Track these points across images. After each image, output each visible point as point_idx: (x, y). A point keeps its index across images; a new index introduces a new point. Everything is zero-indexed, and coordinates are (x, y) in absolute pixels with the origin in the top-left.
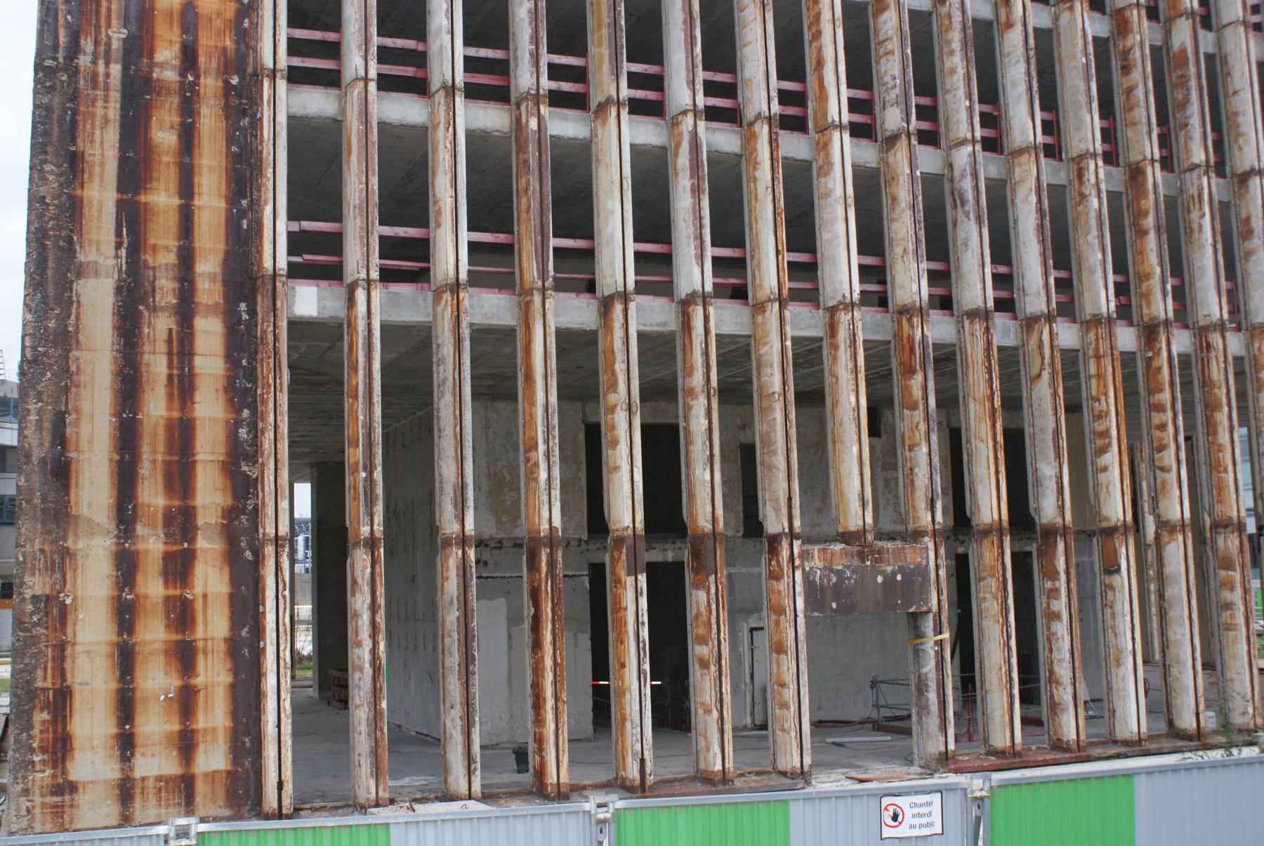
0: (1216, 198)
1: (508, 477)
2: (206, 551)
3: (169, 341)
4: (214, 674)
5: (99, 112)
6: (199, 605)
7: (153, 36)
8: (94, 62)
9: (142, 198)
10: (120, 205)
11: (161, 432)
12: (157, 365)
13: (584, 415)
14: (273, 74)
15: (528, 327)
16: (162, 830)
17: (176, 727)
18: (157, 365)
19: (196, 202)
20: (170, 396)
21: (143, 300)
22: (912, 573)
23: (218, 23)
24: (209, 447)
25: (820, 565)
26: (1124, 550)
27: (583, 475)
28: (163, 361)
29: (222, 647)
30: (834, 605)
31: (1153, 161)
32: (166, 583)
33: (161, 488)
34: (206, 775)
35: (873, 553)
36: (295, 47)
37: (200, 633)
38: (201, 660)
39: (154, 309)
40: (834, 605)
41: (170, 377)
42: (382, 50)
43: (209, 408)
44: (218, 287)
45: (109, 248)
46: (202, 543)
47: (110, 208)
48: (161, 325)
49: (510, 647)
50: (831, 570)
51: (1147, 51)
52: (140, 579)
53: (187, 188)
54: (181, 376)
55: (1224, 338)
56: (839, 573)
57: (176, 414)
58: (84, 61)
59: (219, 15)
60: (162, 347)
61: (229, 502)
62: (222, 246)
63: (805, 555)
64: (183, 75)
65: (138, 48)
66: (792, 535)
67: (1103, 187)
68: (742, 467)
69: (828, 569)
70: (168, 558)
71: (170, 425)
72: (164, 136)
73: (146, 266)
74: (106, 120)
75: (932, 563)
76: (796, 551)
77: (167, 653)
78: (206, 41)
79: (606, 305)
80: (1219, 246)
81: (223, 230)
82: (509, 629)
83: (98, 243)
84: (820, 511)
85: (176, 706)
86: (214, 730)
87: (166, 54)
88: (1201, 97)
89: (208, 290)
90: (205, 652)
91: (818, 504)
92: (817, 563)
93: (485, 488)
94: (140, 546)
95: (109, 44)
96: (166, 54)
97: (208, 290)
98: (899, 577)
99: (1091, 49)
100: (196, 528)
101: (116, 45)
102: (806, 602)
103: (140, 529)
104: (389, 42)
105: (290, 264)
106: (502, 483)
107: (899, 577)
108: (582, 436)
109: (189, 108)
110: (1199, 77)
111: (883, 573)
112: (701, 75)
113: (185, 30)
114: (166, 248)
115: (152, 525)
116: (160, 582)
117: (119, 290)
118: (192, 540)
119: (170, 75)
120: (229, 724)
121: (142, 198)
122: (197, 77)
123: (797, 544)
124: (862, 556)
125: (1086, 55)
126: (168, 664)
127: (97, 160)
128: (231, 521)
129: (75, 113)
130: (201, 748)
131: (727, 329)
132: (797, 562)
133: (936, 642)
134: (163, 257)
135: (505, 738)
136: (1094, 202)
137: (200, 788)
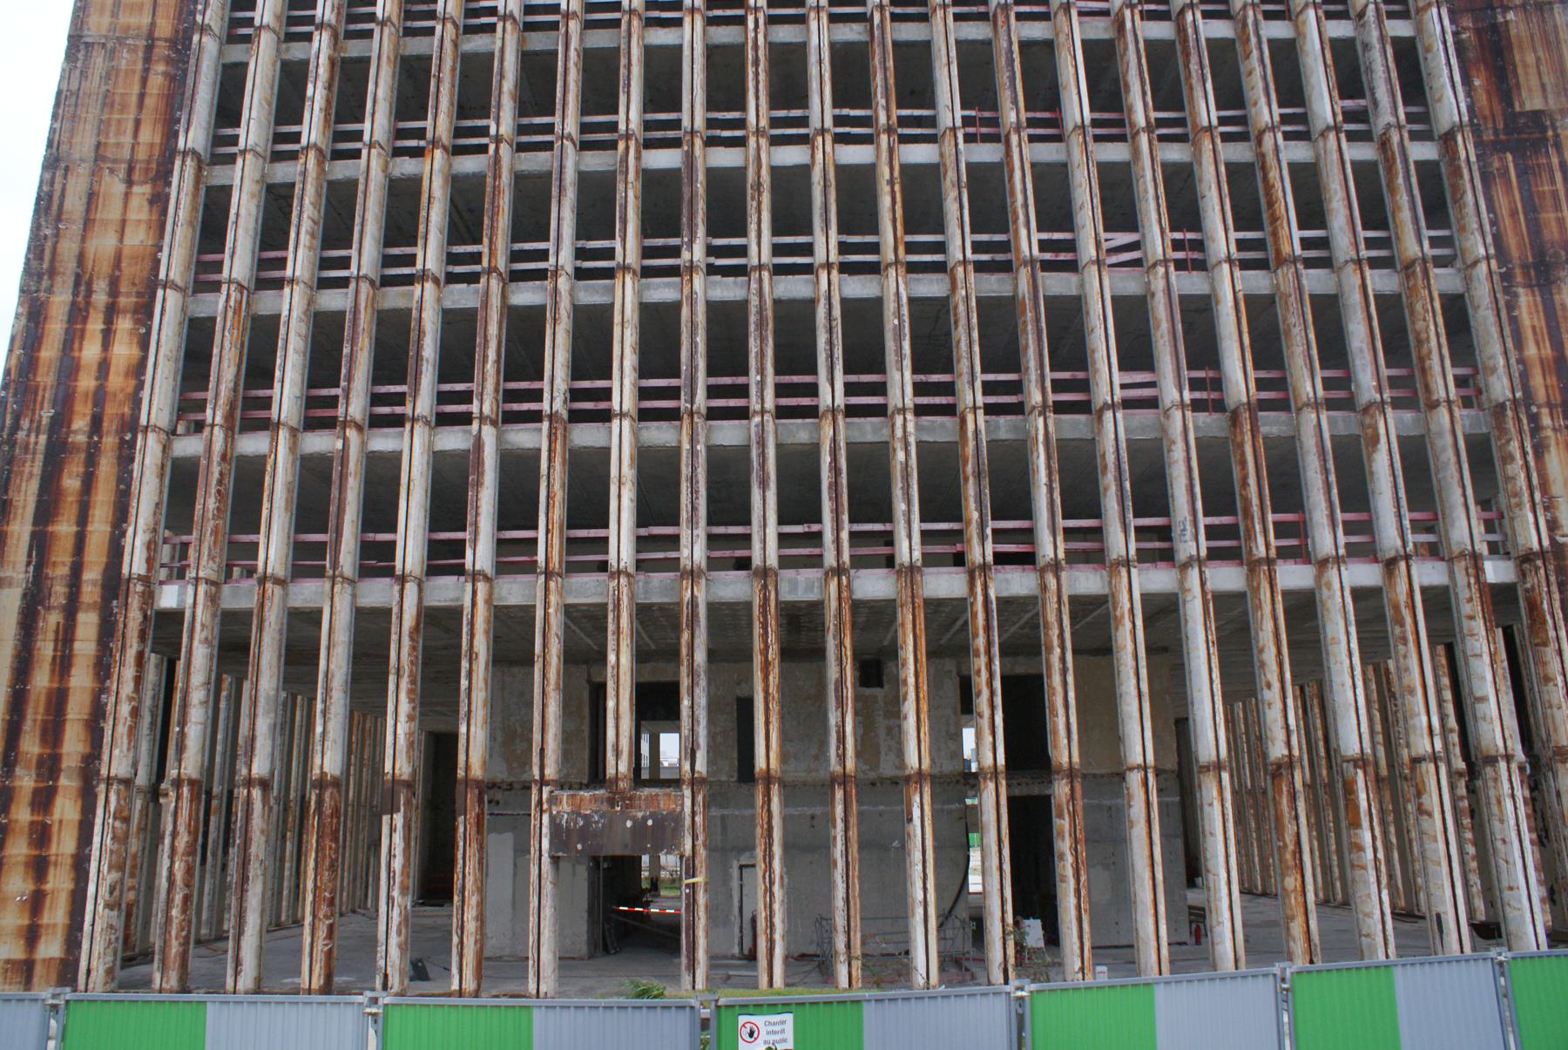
0: (1053, 437)
1: (519, 730)
2: (66, 787)
3: (57, 632)
4: (59, 881)
5: (27, 470)
6: (55, 829)
7: (72, 412)
8: (28, 436)
9: (50, 529)
10: (34, 535)
11: (43, 699)
12: (46, 649)
13: (589, 675)
14: (975, 408)
15: (1256, 591)
16: (359, 999)
17: (26, 922)
18: (46, 649)
19: (89, 528)
20: (53, 671)
21: (41, 603)
22: (664, 818)
23: (121, 396)
24: (77, 709)
25: (568, 809)
26: (917, 799)
27: (586, 728)
28: (51, 646)
29: (69, 861)
30: (579, 847)
31: (975, 408)
32: (33, 810)
33: (37, 741)
34: (44, 960)
35: (623, 799)
36: (919, 389)
37: (53, 849)
38: (51, 871)
39: (49, 609)
40: (579, 847)
41: (54, 658)
42: (985, 384)
43: (81, 679)
44: (98, 590)
45: (21, 566)
46: (63, 781)
47: (26, 537)
48: (52, 620)
49: (515, 874)
50: (579, 814)
51: (974, 303)
52: (13, 808)
53: (83, 519)
54: (63, 657)
55: (1058, 579)
56: (586, 817)
57: (55, 685)
58: (21, 435)
59: (122, 390)
60: (51, 635)
61: (88, 750)
62: (104, 559)
63: (553, 800)
64: (90, 437)
65: (61, 421)
66: (543, 782)
67: (912, 440)
68: (738, 718)
69: (576, 813)
70: (36, 792)
71: (50, 693)
72: (71, 483)
73: (47, 577)
74: (31, 474)
75: (688, 809)
76: (545, 796)
77: (27, 865)
78: (111, 410)
79: (1390, 565)
80: (1056, 485)
81: (106, 546)
82: (515, 857)
83: (14, 563)
84: (816, 758)
85: (28, 906)
86: (55, 925)
87: (80, 423)
88: (1039, 339)
89: (90, 592)
90: (56, 864)
91: (814, 751)
92: (565, 807)
93: (499, 739)
94: (17, 783)
95: (40, 422)
96: (80, 423)
97: (90, 592)
98: (650, 823)
99: (905, 310)
100: (60, 770)
101: (45, 421)
102: (551, 843)
103: (18, 771)
104: (991, 377)
105: (924, 555)
106: (295, 733)
107: (650, 823)
108: (586, 695)
109: (92, 461)
110: (1038, 320)
111: (634, 819)
112: (1049, 375)
113: (95, 405)
114: (63, 564)
115: (28, 768)
116: (28, 810)
117: (25, 595)
118: (56, 779)
119: (81, 438)
120: (67, 921)
121: (50, 529)
122: (101, 437)
123: (546, 790)
124: (612, 802)
125: (899, 317)
126: (26, 873)
127: (21, 504)
128: (87, 765)
129: (10, 472)
130: (43, 939)
131: (1427, 582)
132: (545, 807)
133: (688, 886)
134: (60, 570)
135: (507, 951)
136: (901, 456)
137: (39, 970)
